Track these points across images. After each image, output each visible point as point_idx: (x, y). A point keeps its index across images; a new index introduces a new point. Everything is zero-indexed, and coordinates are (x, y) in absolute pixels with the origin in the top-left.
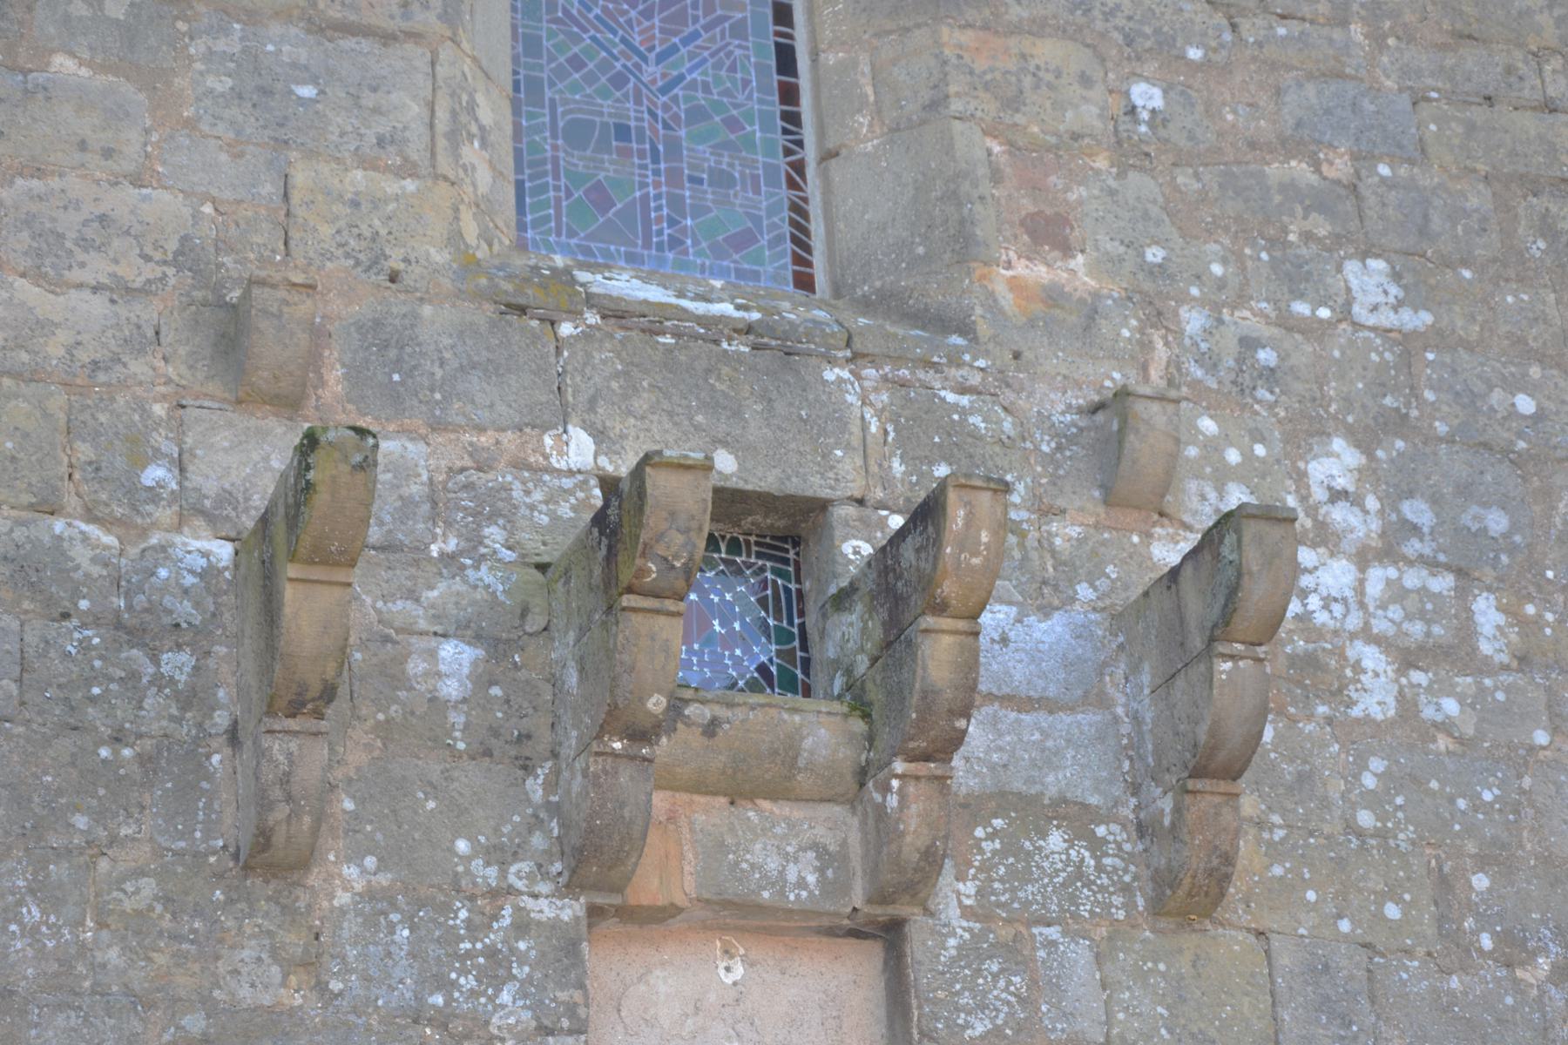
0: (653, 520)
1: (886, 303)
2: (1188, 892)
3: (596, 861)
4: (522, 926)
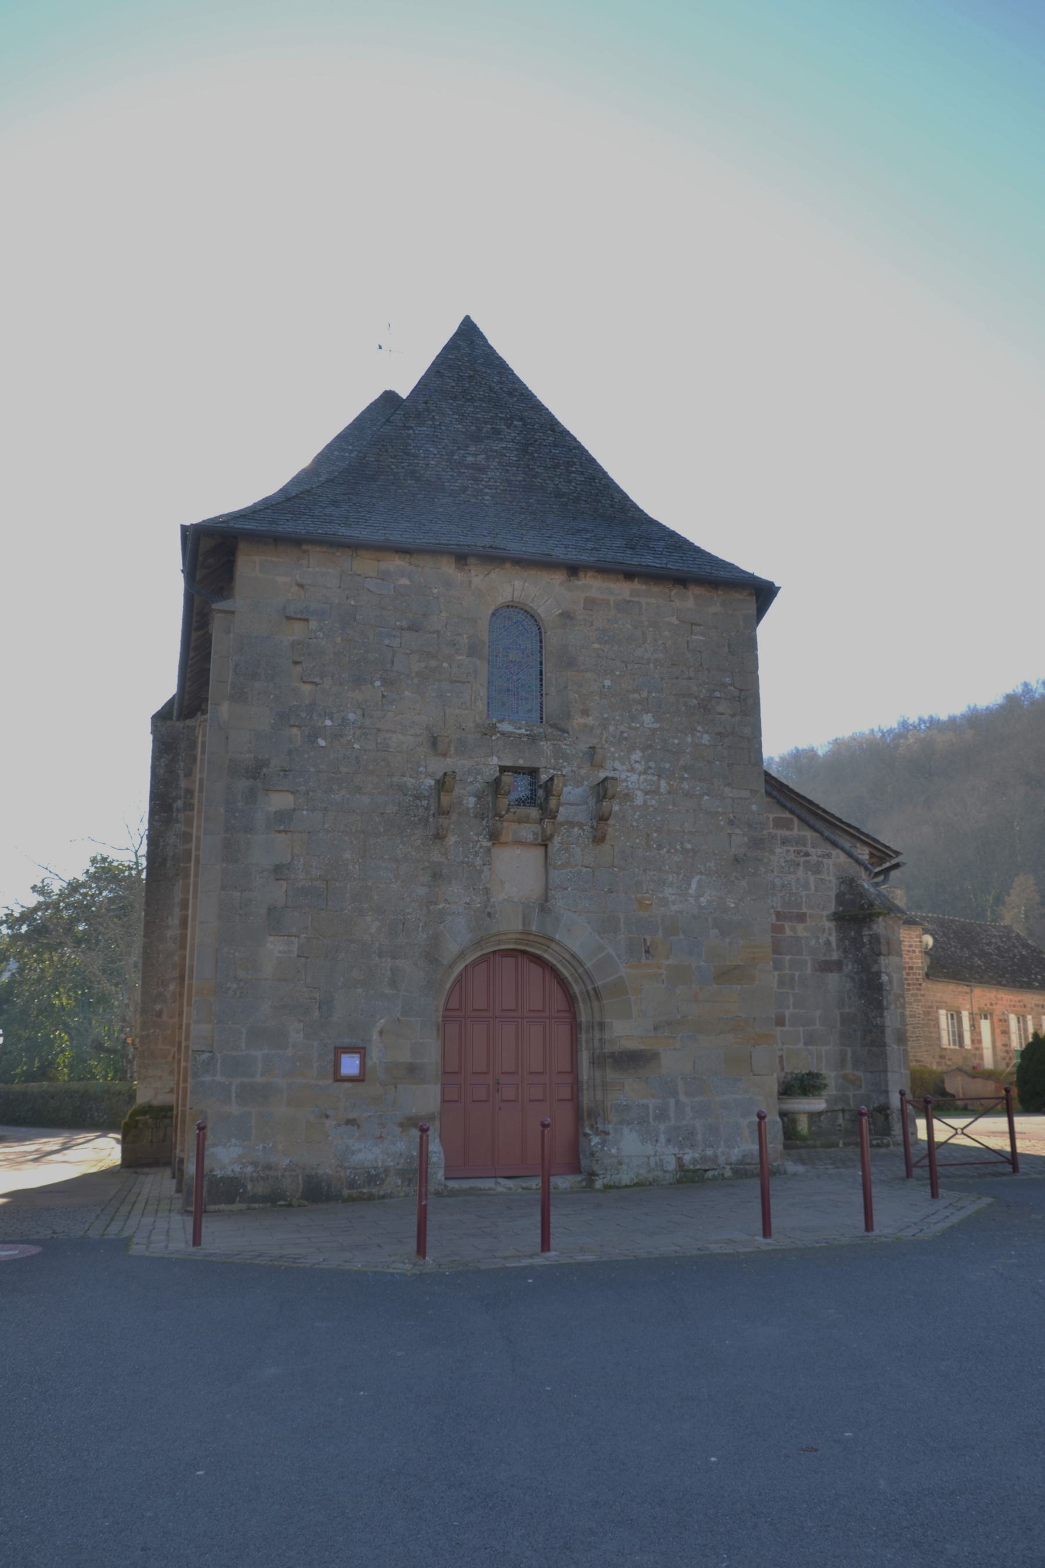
0: (503, 784)
1: (554, 726)
2: (599, 839)
3: (494, 836)
4: (481, 847)
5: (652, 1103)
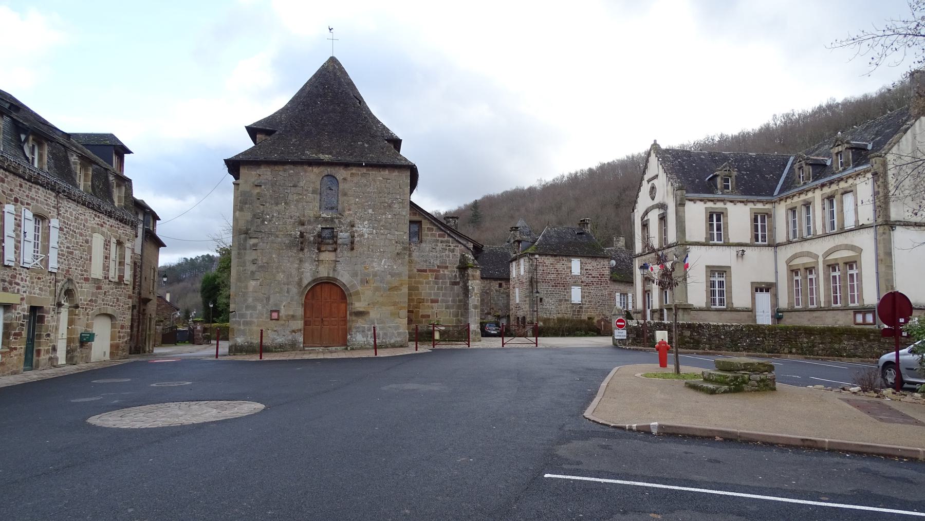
5: (366, 326)
